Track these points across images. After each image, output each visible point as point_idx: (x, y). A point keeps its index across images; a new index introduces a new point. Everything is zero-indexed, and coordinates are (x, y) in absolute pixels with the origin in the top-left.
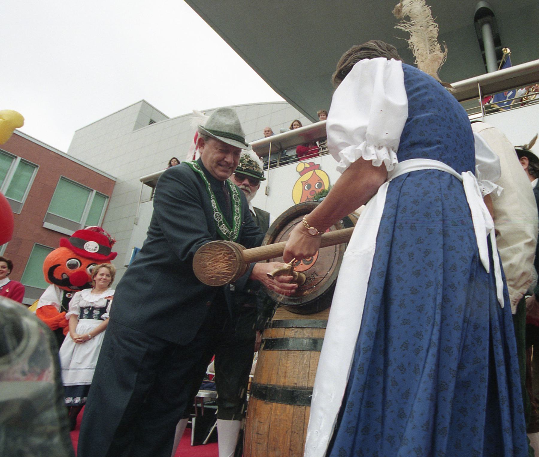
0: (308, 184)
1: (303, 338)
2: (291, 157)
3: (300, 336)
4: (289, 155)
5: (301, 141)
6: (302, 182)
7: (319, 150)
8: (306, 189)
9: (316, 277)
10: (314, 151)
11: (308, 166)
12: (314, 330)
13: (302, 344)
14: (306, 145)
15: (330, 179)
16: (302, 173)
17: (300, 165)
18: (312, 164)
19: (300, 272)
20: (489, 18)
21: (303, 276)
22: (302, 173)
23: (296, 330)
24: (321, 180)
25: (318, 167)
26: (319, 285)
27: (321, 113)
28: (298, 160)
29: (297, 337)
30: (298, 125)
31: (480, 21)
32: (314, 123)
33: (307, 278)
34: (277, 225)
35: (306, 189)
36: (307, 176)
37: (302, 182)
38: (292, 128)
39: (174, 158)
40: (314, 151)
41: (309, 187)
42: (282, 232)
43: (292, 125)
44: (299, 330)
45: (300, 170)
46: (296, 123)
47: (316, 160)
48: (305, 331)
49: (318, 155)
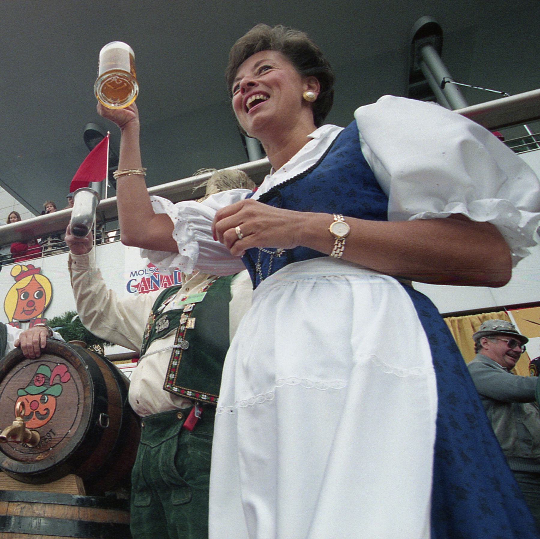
0: (24, 292)
1: (32, 517)
2: (5, 256)
3: (29, 514)
4: (4, 254)
5: (19, 236)
6: (17, 289)
7: (41, 250)
8: (22, 298)
9: (53, 436)
10: (34, 251)
11: (26, 269)
12: (47, 507)
13: (31, 525)
14: (25, 242)
15: (54, 289)
16: (17, 278)
17: (15, 268)
18: (30, 267)
19: (32, 430)
20: (433, 39)
21: (37, 434)
22: (17, 278)
23: (23, 505)
24: (42, 288)
25: (38, 271)
26: (57, 447)
27: (47, 204)
28: (13, 262)
29: (24, 515)
30: (15, 218)
31: (421, 41)
32: (37, 216)
33: (41, 438)
34: (4, 367)
35: (22, 298)
36: (25, 282)
37: (17, 289)
38: (9, 222)
39: (14, 212)
40: (34, 251)
41: (26, 295)
42: (9, 376)
43: (9, 218)
44: (27, 505)
45: (15, 275)
46: (13, 215)
47: (36, 263)
48: (35, 507)
49: (40, 256)
